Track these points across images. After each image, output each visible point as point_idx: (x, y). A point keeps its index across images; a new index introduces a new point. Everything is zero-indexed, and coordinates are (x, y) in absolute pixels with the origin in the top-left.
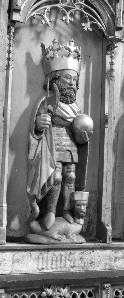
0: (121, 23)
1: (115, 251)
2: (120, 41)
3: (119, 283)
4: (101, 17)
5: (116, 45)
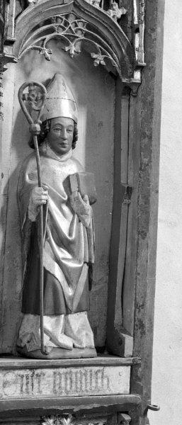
0: (13, 34)
1: (5, 372)
2: (11, 60)
3: (10, 419)
4: (105, 40)
5: (5, 67)
